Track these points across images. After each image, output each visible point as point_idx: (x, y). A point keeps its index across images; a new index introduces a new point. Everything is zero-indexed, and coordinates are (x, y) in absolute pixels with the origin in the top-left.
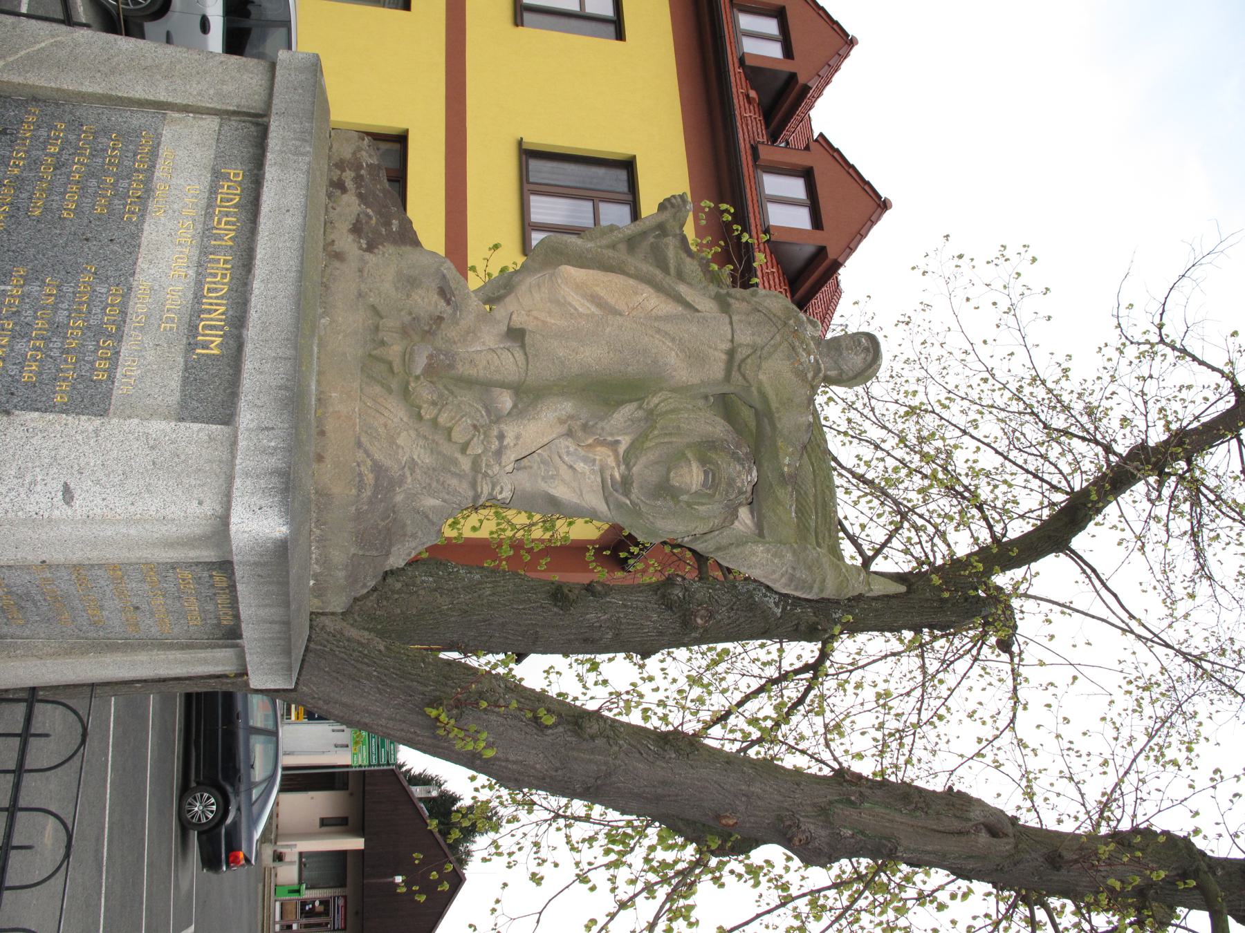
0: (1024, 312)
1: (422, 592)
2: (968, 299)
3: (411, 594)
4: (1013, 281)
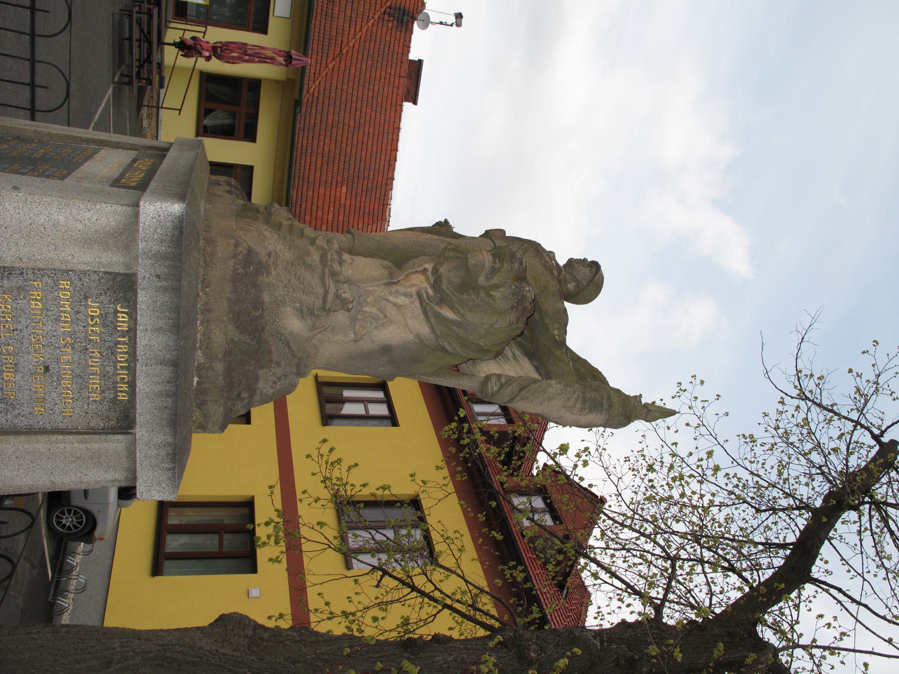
0: (710, 419)
1: (288, 643)
2: (669, 428)
3: (279, 642)
4: (693, 403)
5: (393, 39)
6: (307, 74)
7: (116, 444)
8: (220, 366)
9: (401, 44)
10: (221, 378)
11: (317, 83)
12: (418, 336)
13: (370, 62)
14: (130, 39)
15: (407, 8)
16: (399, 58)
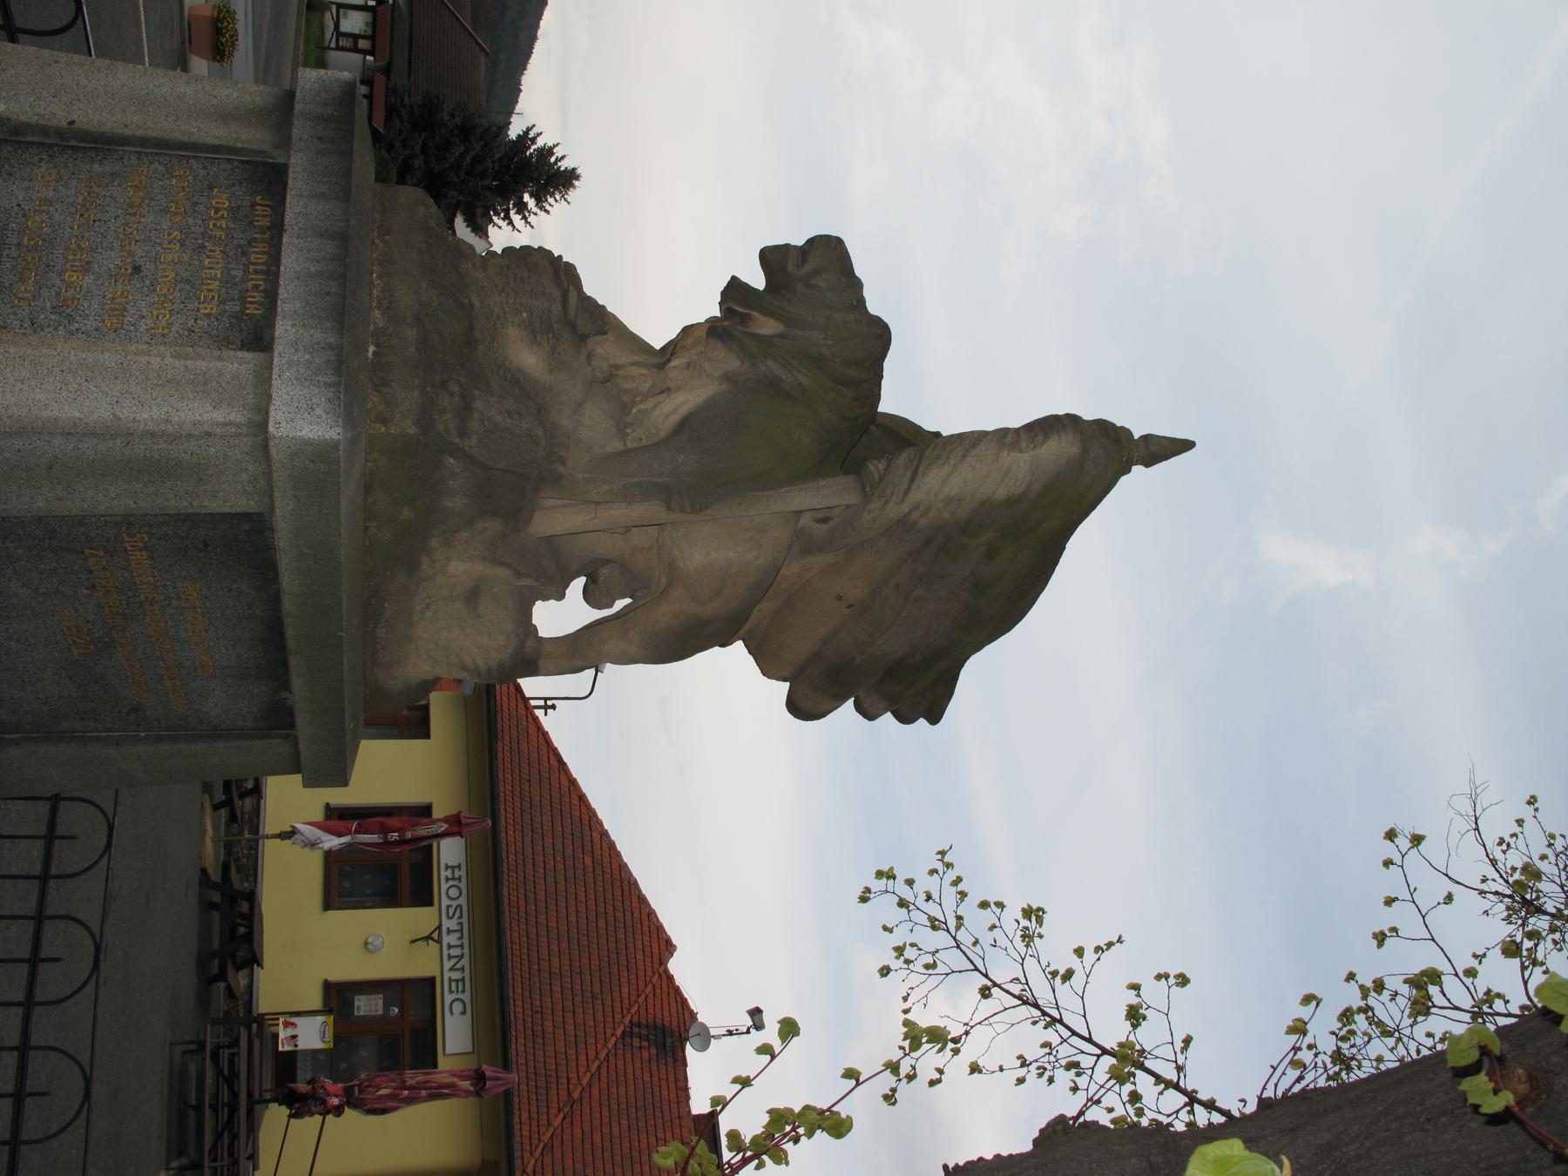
5: (655, 1079)
6: (518, 1139)
7: (240, 364)
8: (410, 333)
9: (672, 1085)
10: (412, 349)
11: (537, 1154)
12: (728, 377)
13: (624, 1122)
14: (199, 1108)
15: (667, 1024)
16: (675, 1111)
